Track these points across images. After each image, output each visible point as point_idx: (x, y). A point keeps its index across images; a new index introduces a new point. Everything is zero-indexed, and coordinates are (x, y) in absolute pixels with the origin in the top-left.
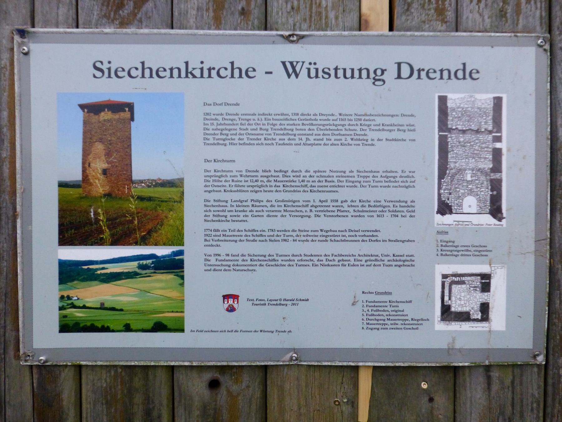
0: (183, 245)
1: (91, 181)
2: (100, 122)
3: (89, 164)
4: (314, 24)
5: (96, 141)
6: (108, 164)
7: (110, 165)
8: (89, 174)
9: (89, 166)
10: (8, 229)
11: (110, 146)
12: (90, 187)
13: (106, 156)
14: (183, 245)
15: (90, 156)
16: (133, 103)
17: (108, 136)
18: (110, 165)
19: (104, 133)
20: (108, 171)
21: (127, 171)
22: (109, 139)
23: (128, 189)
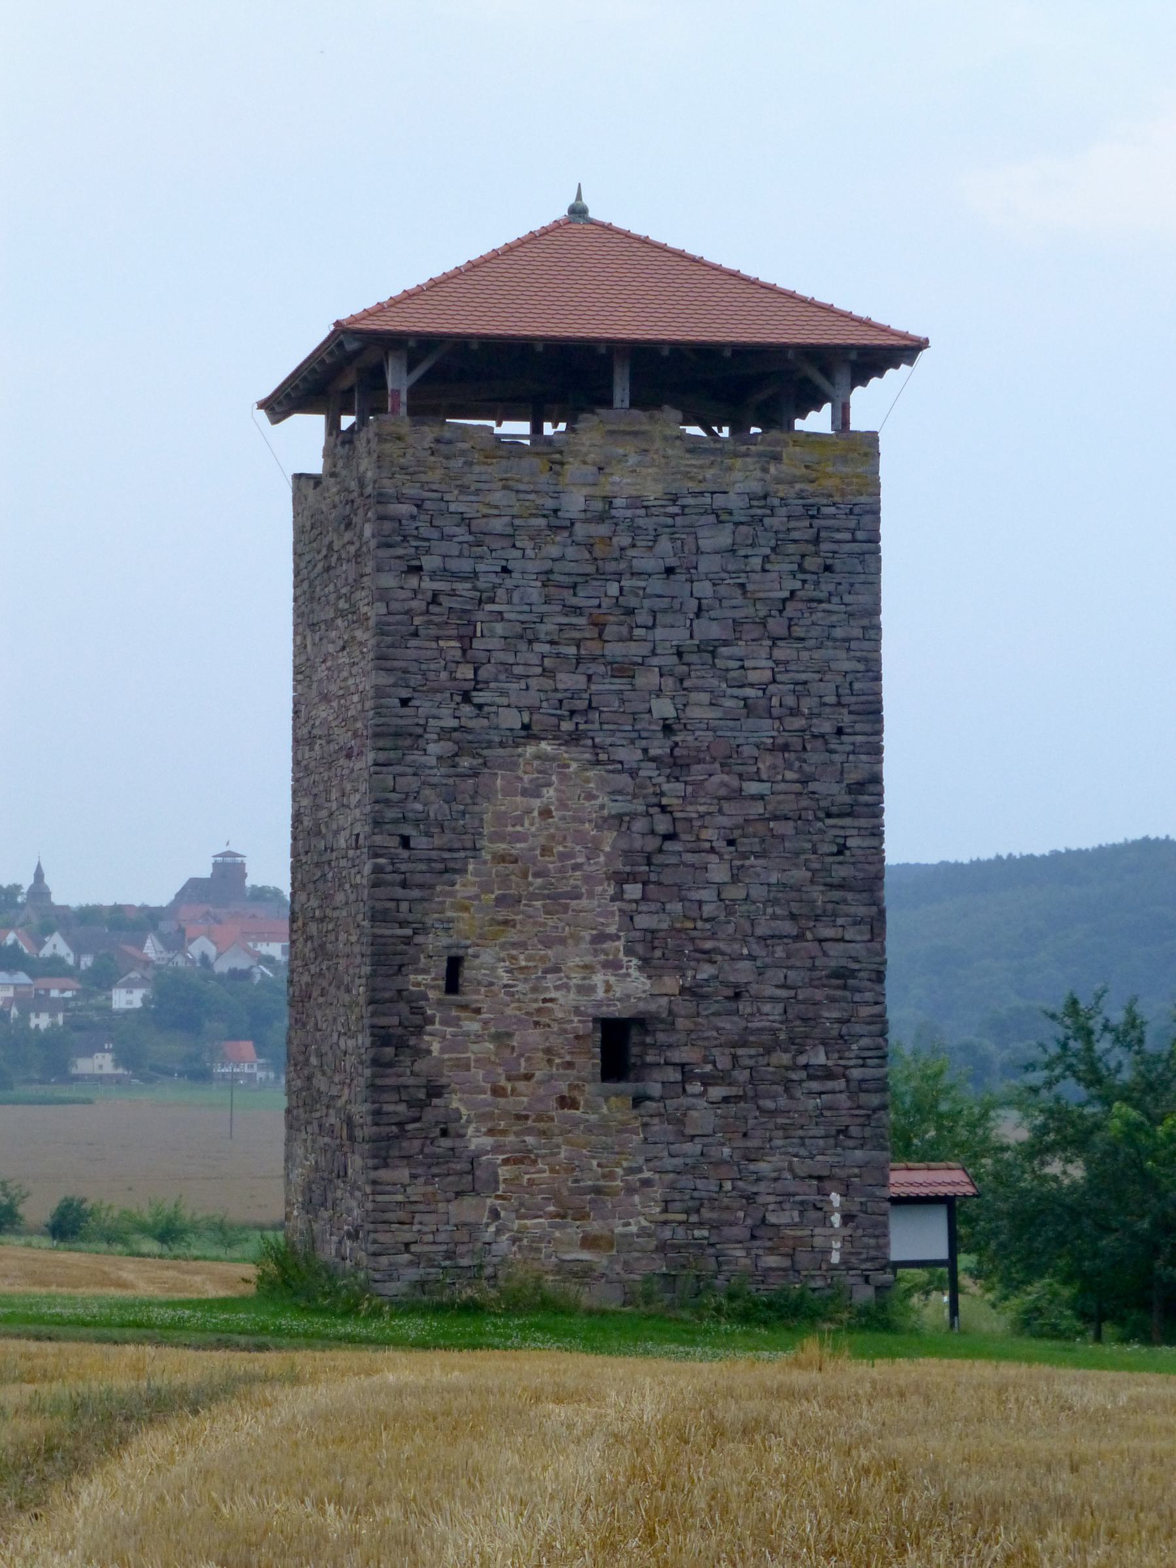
0: (634, 404)
1: (477, 1140)
2: (558, 523)
3: (455, 965)
4: (1138, 1406)
5: (528, 732)
6: (646, 964)
7: (671, 984)
8: (449, 1076)
9: (452, 983)
10: (814, 1509)
11: (673, 790)
12: (465, 1210)
13: (633, 891)
14: (634, 404)
15: (465, 887)
16: (876, 433)
17: (648, 679)
18: (671, 984)
19: (615, 650)
20: (635, 1036)
21: (837, 1042)
22: (664, 708)
23: (847, 1218)
